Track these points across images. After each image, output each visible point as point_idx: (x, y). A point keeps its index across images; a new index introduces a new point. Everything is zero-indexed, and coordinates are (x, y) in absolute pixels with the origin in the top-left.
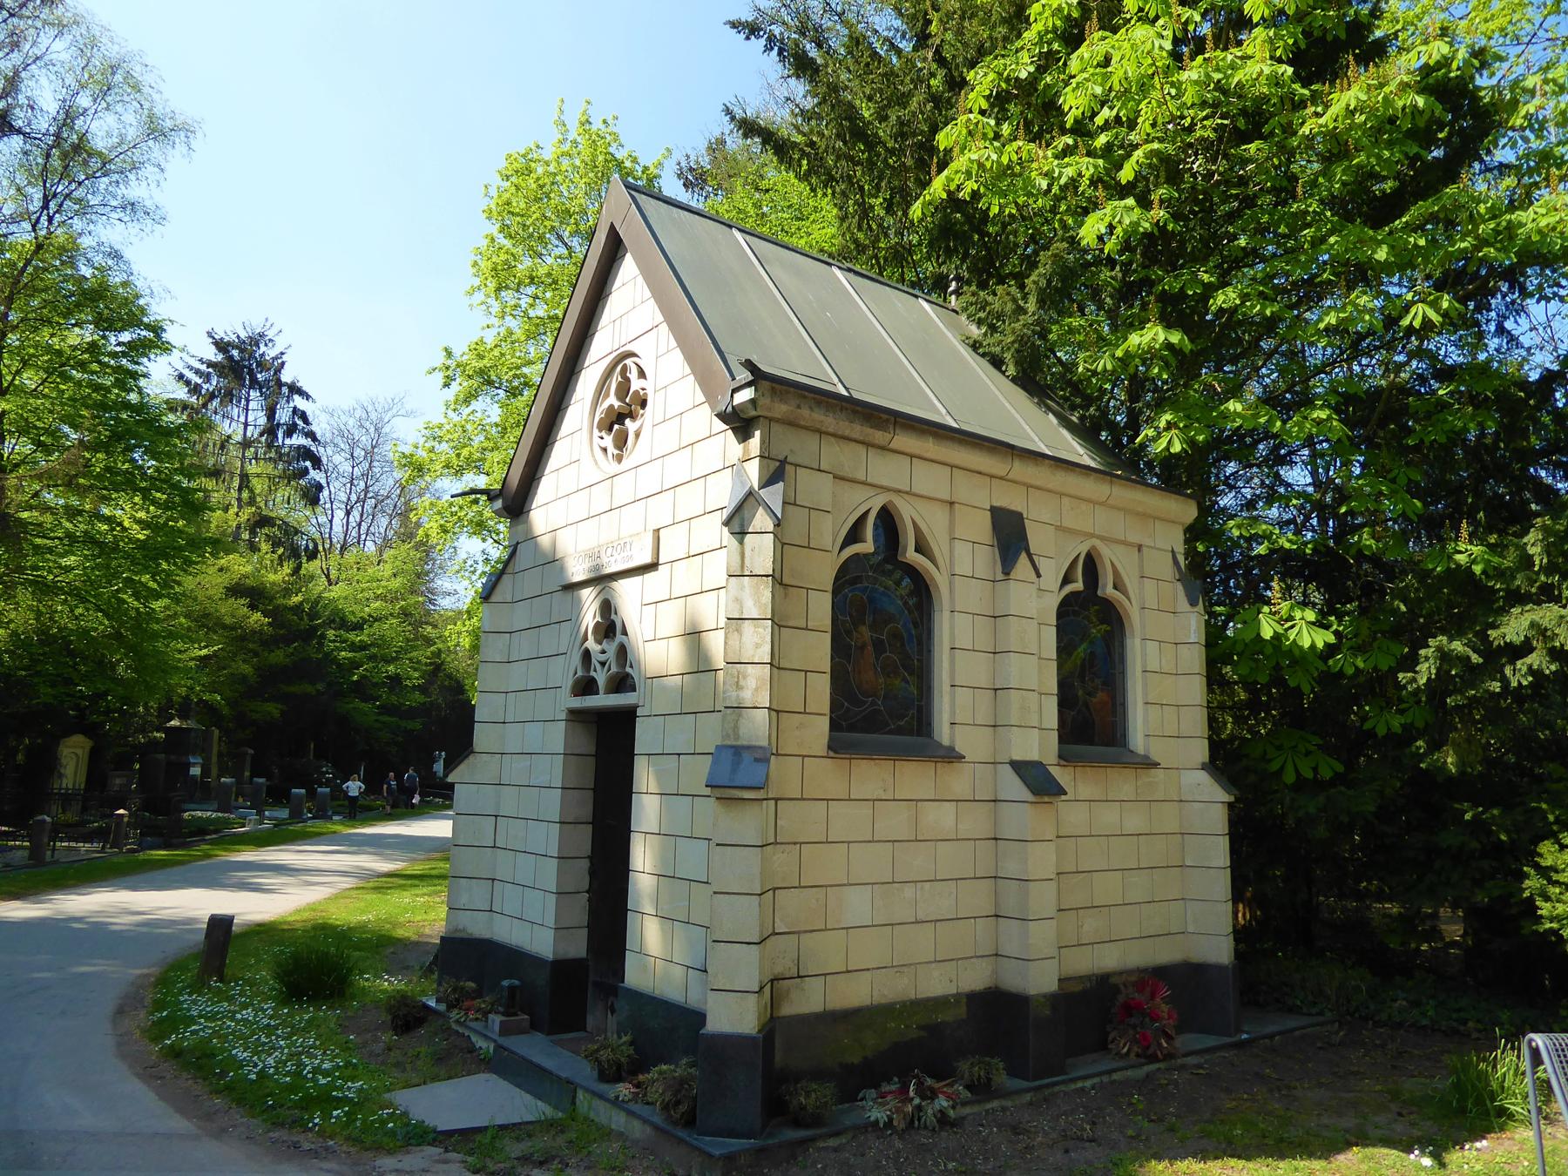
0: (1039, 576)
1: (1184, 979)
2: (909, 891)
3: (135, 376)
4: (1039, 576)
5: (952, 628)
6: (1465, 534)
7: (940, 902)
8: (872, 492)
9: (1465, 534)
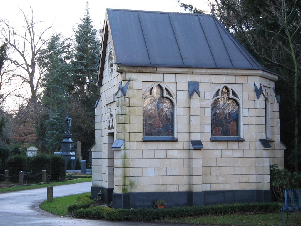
0: (200, 97)
1: (258, 194)
2: (165, 169)
3: (221, 214)
4: (200, 97)
5: (243, 112)
6: (86, 106)
7: (175, 172)
8: (153, 83)
9: (86, 106)
